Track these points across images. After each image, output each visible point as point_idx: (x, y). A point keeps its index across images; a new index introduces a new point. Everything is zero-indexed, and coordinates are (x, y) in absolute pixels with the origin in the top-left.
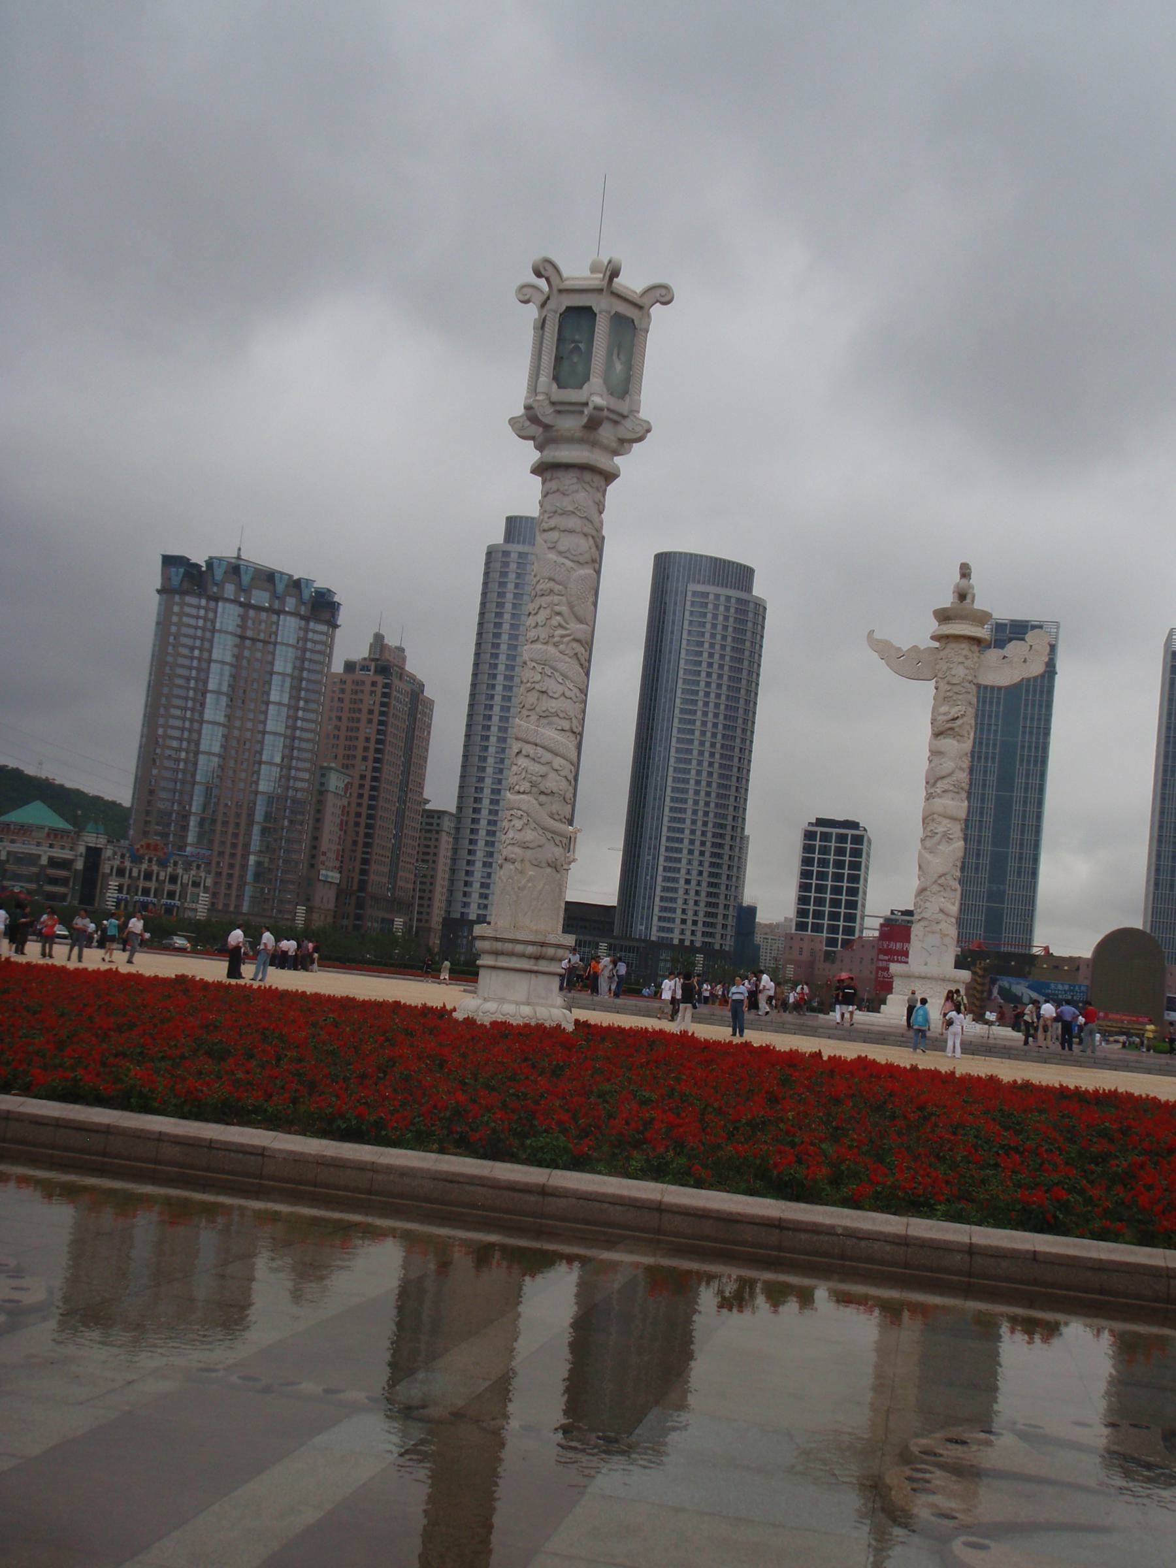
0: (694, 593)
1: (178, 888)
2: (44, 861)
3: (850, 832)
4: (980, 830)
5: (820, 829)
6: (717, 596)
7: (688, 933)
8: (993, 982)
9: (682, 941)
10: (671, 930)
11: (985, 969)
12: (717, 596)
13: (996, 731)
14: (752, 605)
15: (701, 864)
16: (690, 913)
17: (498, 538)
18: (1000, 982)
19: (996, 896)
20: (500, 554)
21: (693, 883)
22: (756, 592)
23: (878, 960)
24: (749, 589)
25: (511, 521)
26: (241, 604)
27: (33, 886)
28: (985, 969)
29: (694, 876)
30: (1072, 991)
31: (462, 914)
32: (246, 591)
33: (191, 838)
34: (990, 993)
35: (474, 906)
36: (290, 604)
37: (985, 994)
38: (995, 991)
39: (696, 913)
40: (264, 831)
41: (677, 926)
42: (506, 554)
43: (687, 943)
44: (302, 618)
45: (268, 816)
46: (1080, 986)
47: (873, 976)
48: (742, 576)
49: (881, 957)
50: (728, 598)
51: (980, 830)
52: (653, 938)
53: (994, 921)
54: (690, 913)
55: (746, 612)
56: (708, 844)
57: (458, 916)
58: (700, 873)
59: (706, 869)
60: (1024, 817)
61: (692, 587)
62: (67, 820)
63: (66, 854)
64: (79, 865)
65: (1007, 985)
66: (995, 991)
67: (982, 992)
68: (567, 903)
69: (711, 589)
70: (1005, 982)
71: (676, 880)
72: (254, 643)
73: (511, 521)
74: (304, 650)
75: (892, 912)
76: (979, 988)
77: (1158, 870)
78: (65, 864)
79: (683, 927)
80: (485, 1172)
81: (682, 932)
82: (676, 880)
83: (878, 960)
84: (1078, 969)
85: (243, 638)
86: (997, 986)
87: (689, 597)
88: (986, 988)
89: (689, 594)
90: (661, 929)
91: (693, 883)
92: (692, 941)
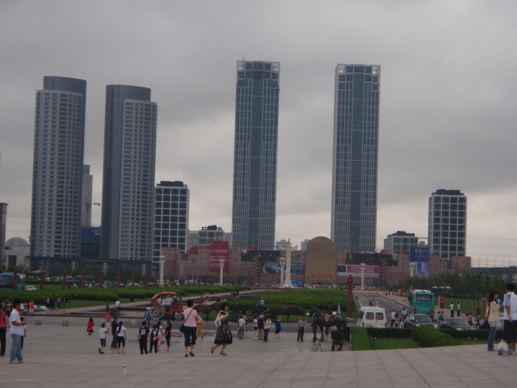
0: (127, 104)
3: (179, 188)
4: (244, 178)
5: (163, 187)
7: (134, 255)
8: (263, 264)
9: (132, 258)
10: (126, 254)
11: (259, 259)
12: (137, 104)
13: (249, 123)
14: (152, 106)
15: (137, 223)
16: (134, 246)
17: (41, 87)
18: (266, 265)
19: (254, 214)
20: (44, 94)
21: (135, 232)
23: (210, 258)
25: (46, 79)
28: (259, 259)
29: (135, 229)
30: (298, 266)
31: (40, 255)
34: (262, 270)
35: (45, 251)
37: (259, 271)
38: (264, 269)
39: (137, 246)
41: (129, 252)
42: (47, 94)
43: (134, 259)
46: (301, 264)
47: (208, 266)
49: (211, 257)
50: (142, 105)
51: (244, 178)
52: (119, 258)
53: (254, 228)
54: (134, 246)
55: (149, 110)
56: (140, 215)
57: (38, 256)
58: (137, 228)
59: (140, 225)
60: (266, 170)
61: (126, 101)
65: (269, 266)
66: (264, 269)
67: (258, 269)
69: (134, 101)
70: (268, 264)
71: (127, 232)
73: (46, 79)
75: (203, 229)
76: (257, 268)
77: (337, 195)
79: (132, 252)
81: (132, 254)
82: (127, 232)
83: (210, 258)
84: (299, 256)
86: (264, 267)
87: (125, 105)
88: (260, 267)
89: (125, 104)
90: (122, 254)
91: (135, 232)
92: (136, 258)
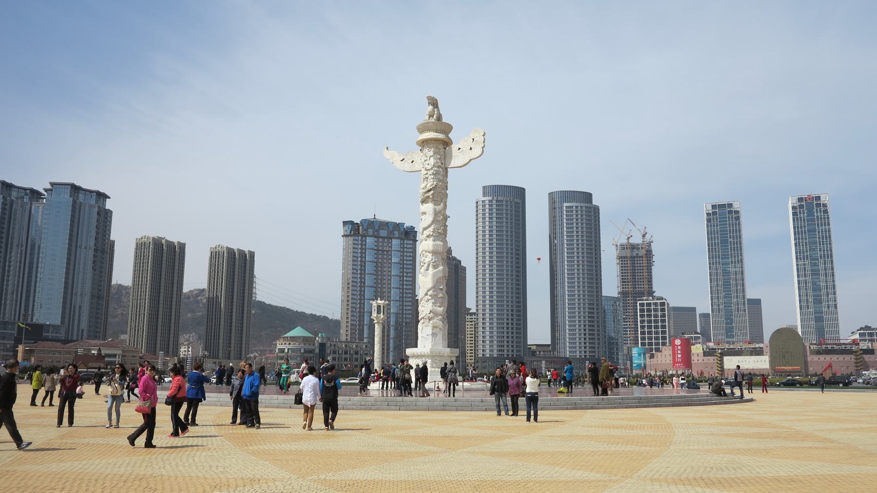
1: (359, 356)
2: (302, 351)
6: (577, 207)
12: (577, 207)
19: (819, 319)
22: (594, 203)
24: (591, 202)
26: (376, 237)
27: (377, 365)
32: (378, 231)
33: (365, 335)
36: (396, 234)
40: (396, 329)
44: (401, 239)
45: (397, 322)
48: (587, 197)
62: (307, 330)
63: (311, 347)
64: (317, 351)
68: (748, 300)
72: (382, 254)
74: (404, 252)
78: (312, 351)
80: (425, 308)
85: (378, 250)
